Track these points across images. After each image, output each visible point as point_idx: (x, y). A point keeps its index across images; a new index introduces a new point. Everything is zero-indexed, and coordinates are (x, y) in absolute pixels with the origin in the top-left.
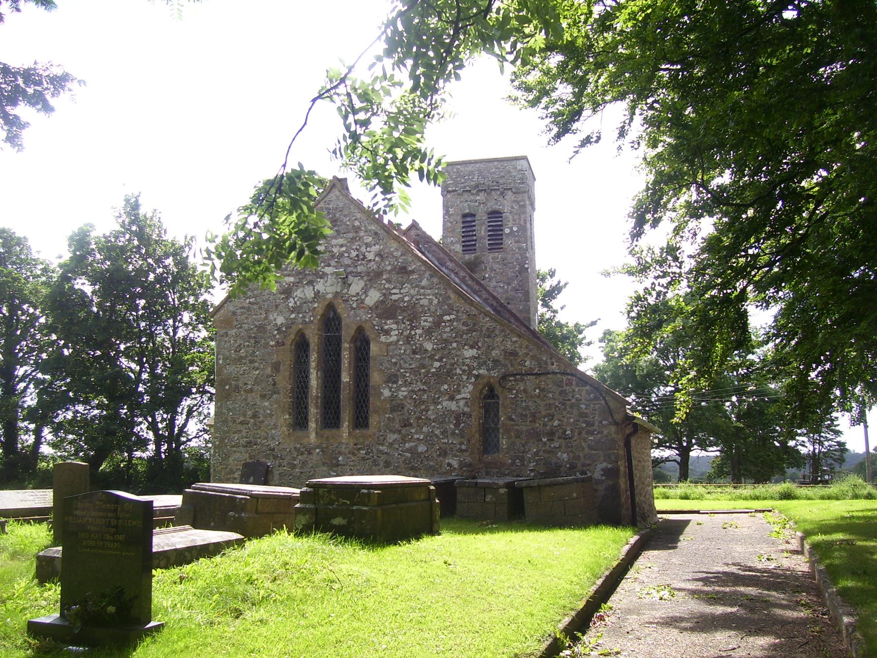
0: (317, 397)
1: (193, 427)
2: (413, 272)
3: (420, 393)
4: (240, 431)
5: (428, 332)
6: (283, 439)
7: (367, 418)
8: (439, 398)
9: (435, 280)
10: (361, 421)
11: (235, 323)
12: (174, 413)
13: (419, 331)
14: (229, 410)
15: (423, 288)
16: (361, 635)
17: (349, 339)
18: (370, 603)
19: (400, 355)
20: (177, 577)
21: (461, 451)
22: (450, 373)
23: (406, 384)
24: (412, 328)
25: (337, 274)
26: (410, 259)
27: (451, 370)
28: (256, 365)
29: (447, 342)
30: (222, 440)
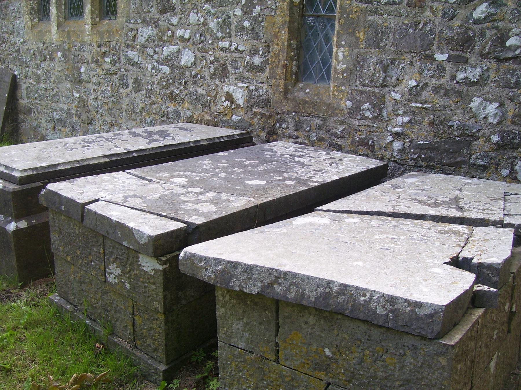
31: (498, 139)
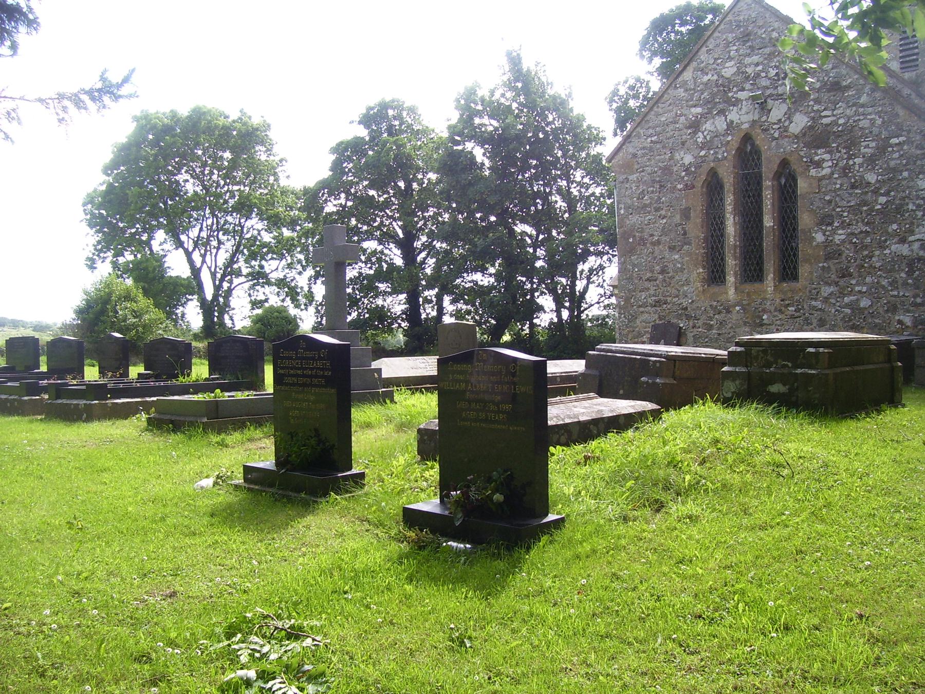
0: (735, 246)
1: (593, 295)
2: (848, 87)
3: (862, 235)
4: (648, 289)
5: (871, 161)
6: (697, 296)
7: (795, 268)
8: (886, 241)
9: (878, 95)
10: (788, 272)
11: (636, 167)
12: (574, 279)
13: (858, 160)
14: (634, 266)
15: (863, 106)
16: (830, 544)
17: (771, 176)
18: (835, 495)
19: (835, 191)
20: (580, 457)
21: (915, 305)
22: (899, 210)
23: (843, 225)
24: (849, 158)
25: (754, 98)
26: (844, 72)
27: (902, 205)
28: (663, 212)
29: (894, 170)
30: (627, 300)
31: (600, 118)
